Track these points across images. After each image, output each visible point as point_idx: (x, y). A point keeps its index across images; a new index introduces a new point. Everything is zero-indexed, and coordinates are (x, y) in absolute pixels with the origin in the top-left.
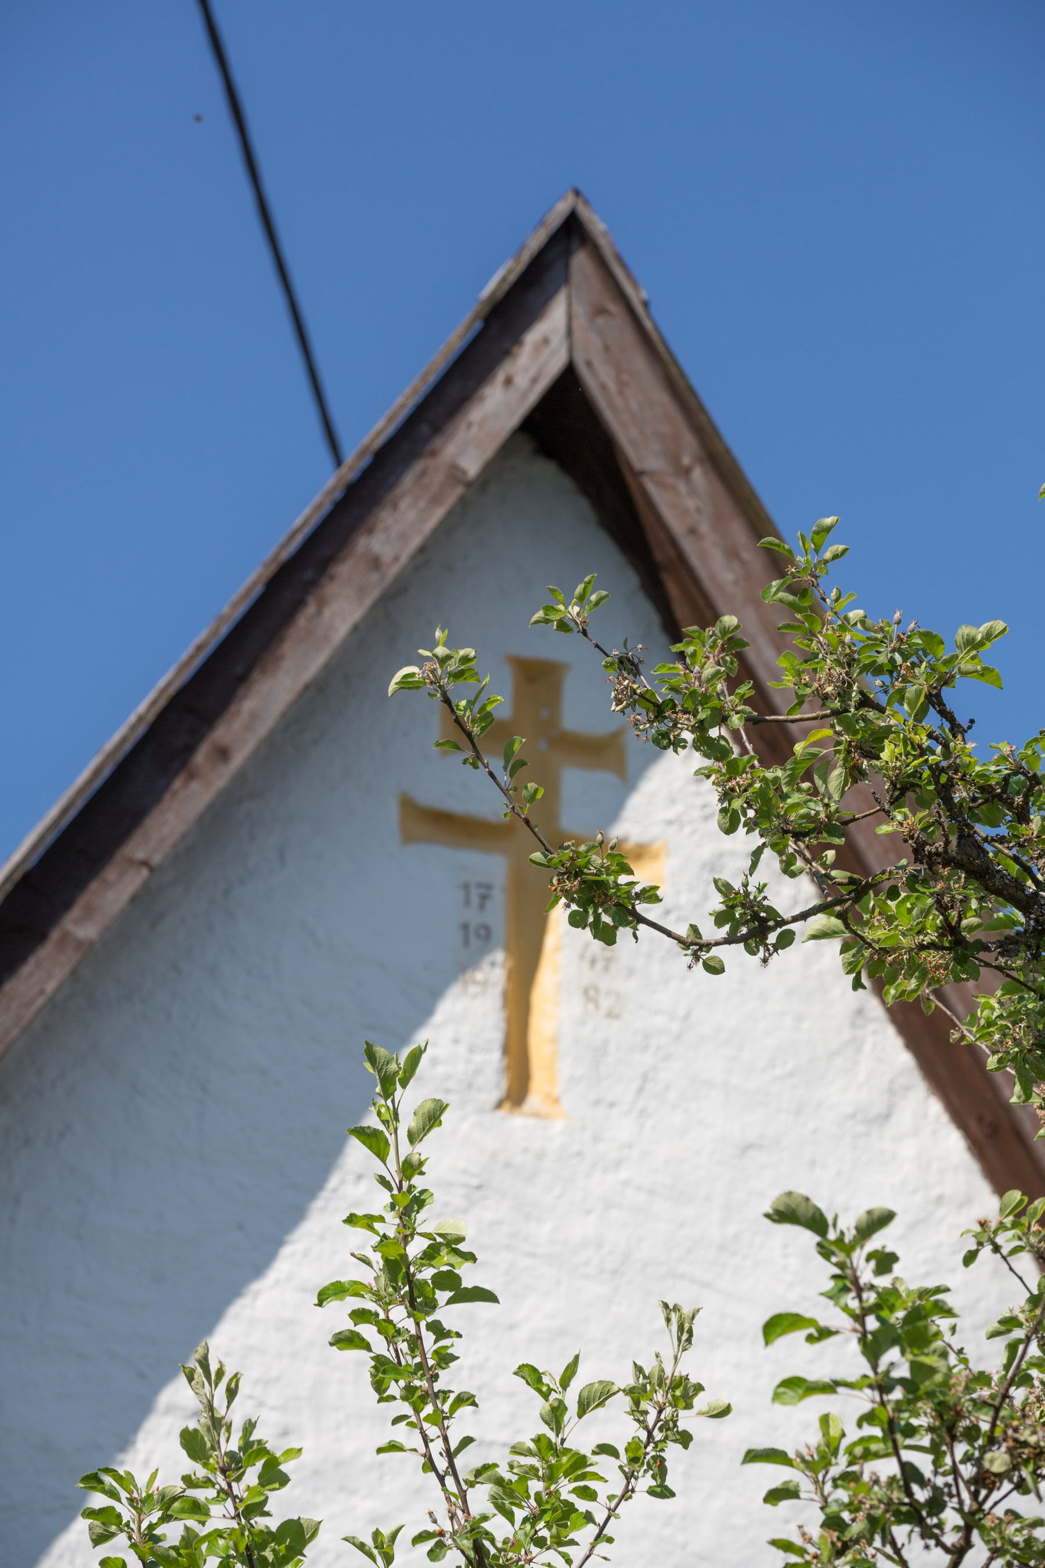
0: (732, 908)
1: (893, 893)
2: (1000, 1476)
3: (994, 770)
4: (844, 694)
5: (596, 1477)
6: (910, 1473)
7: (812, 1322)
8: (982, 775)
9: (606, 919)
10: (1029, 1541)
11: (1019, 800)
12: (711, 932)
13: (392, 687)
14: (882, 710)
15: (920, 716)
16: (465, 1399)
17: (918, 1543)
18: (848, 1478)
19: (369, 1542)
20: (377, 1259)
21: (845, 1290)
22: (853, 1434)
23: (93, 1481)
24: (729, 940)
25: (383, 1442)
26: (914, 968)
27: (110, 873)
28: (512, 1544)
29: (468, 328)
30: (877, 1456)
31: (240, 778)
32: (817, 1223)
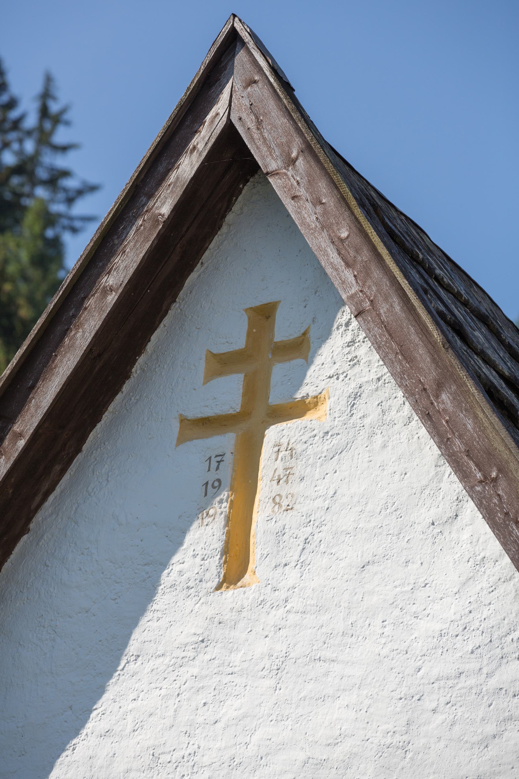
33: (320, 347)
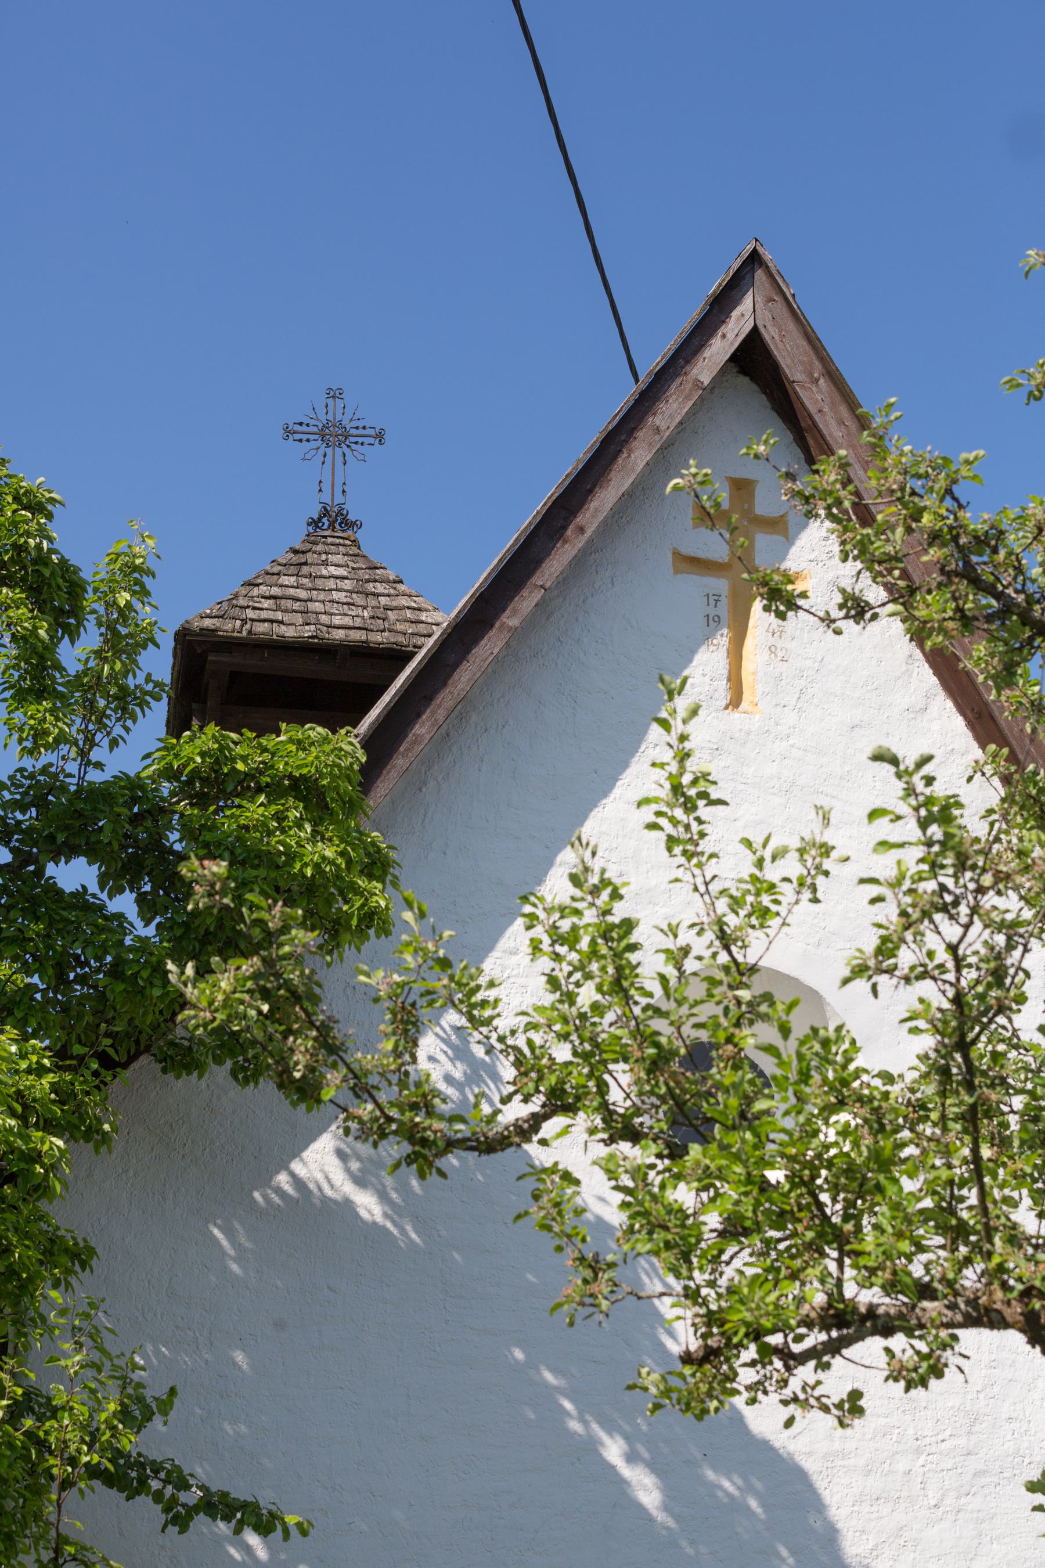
0: (846, 601)
1: (929, 592)
2: (988, 889)
3: (981, 528)
4: (902, 489)
5: (780, 893)
6: (943, 888)
7: (892, 812)
8: (974, 530)
9: (782, 608)
10: (1003, 920)
11: (993, 542)
12: (836, 613)
13: (669, 489)
14: (922, 497)
15: (942, 500)
16: (713, 856)
17: (947, 921)
18: (911, 891)
19: (666, 928)
20: (667, 786)
21: (909, 795)
22: (914, 869)
23: (525, 899)
24: (847, 617)
25: (672, 878)
26: (941, 630)
27: (525, 592)
28: (740, 928)
29: (702, 310)
30: (925, 879)
31: (590, 541)
32: (894, 761)
33: (799, 533)
